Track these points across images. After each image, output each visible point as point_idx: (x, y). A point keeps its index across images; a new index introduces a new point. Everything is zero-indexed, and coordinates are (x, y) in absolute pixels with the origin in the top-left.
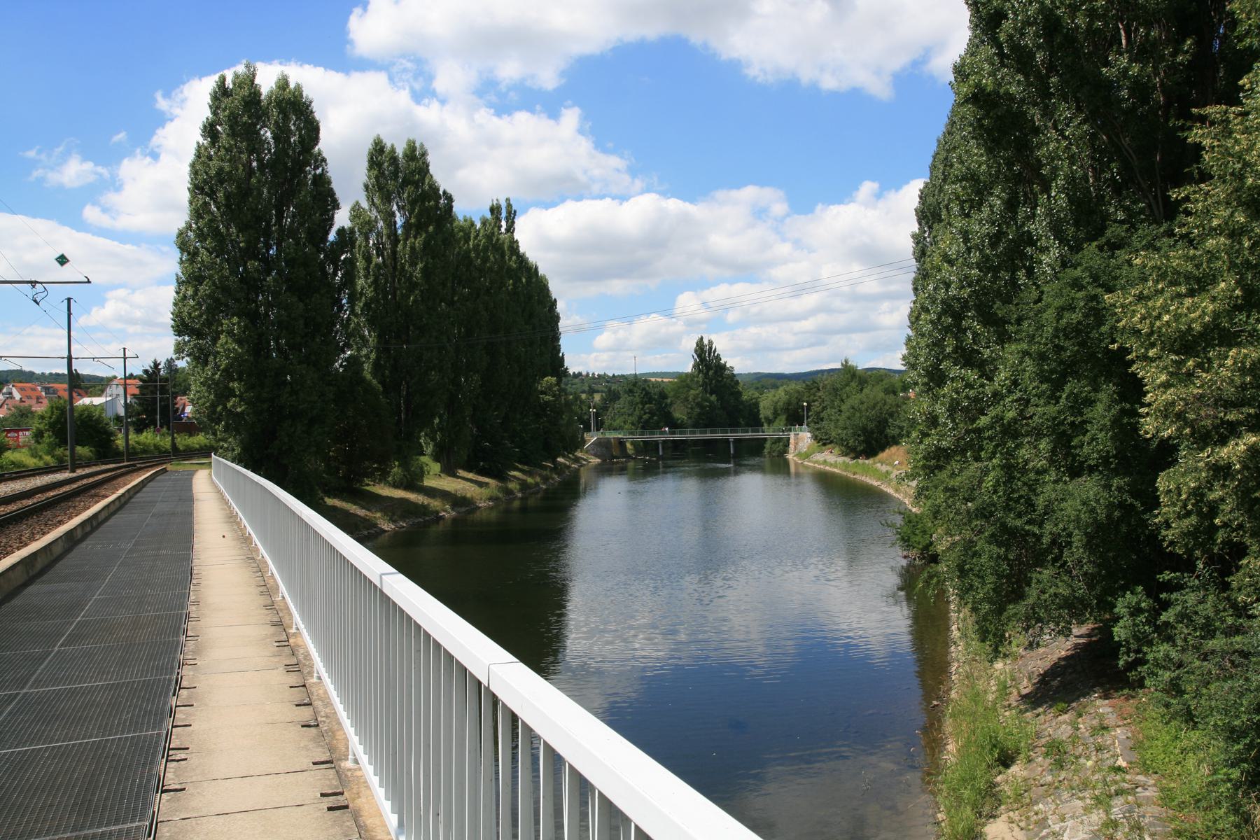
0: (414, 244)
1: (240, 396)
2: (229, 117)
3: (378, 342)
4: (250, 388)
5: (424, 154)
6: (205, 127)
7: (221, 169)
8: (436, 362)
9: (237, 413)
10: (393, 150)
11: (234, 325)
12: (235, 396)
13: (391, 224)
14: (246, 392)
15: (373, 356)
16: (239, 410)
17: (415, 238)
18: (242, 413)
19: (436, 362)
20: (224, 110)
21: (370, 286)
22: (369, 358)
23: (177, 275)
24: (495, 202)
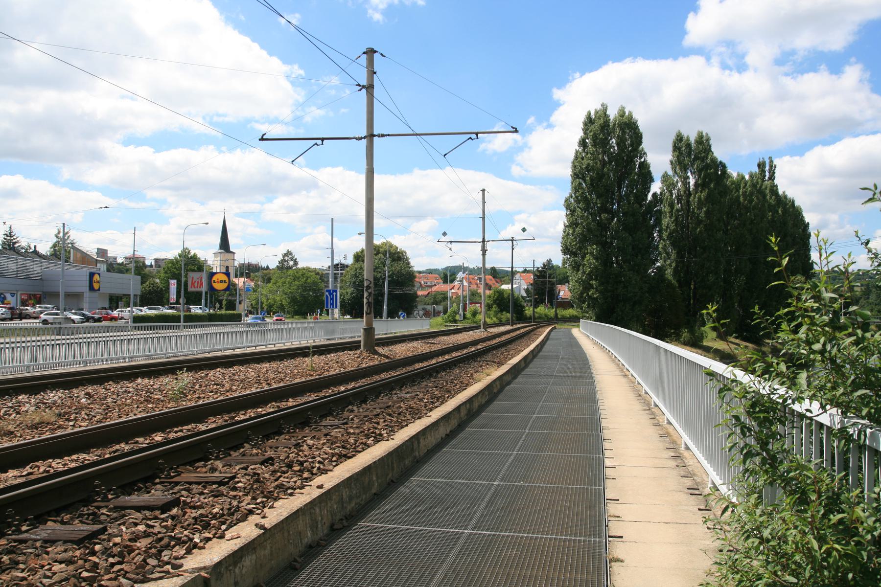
0: (700, 196)
1: (596, 289)
2: (593, 136)
3: (677, 256)
4: (601, 284)
5: (708, 140)
6: (580, 141)
7: (588, 165)
8: (713, 268)
9: (594, 298)
10: (688, 139)
11: (594, 249)
12: (593, 288)
13: (686, 183)
14: (599, 286)
15: (674, 265)
16: (595, 296)
17: (701, 192)
18: (597, 297)
19: (713, 268)
20: (590, 132)
21: (672, 223)
22: (672, 266)
23: (564, 222)
24: (761, 160)
